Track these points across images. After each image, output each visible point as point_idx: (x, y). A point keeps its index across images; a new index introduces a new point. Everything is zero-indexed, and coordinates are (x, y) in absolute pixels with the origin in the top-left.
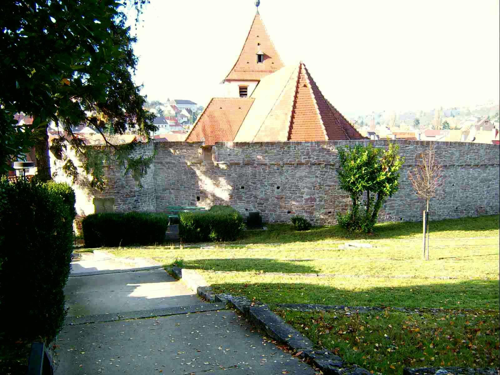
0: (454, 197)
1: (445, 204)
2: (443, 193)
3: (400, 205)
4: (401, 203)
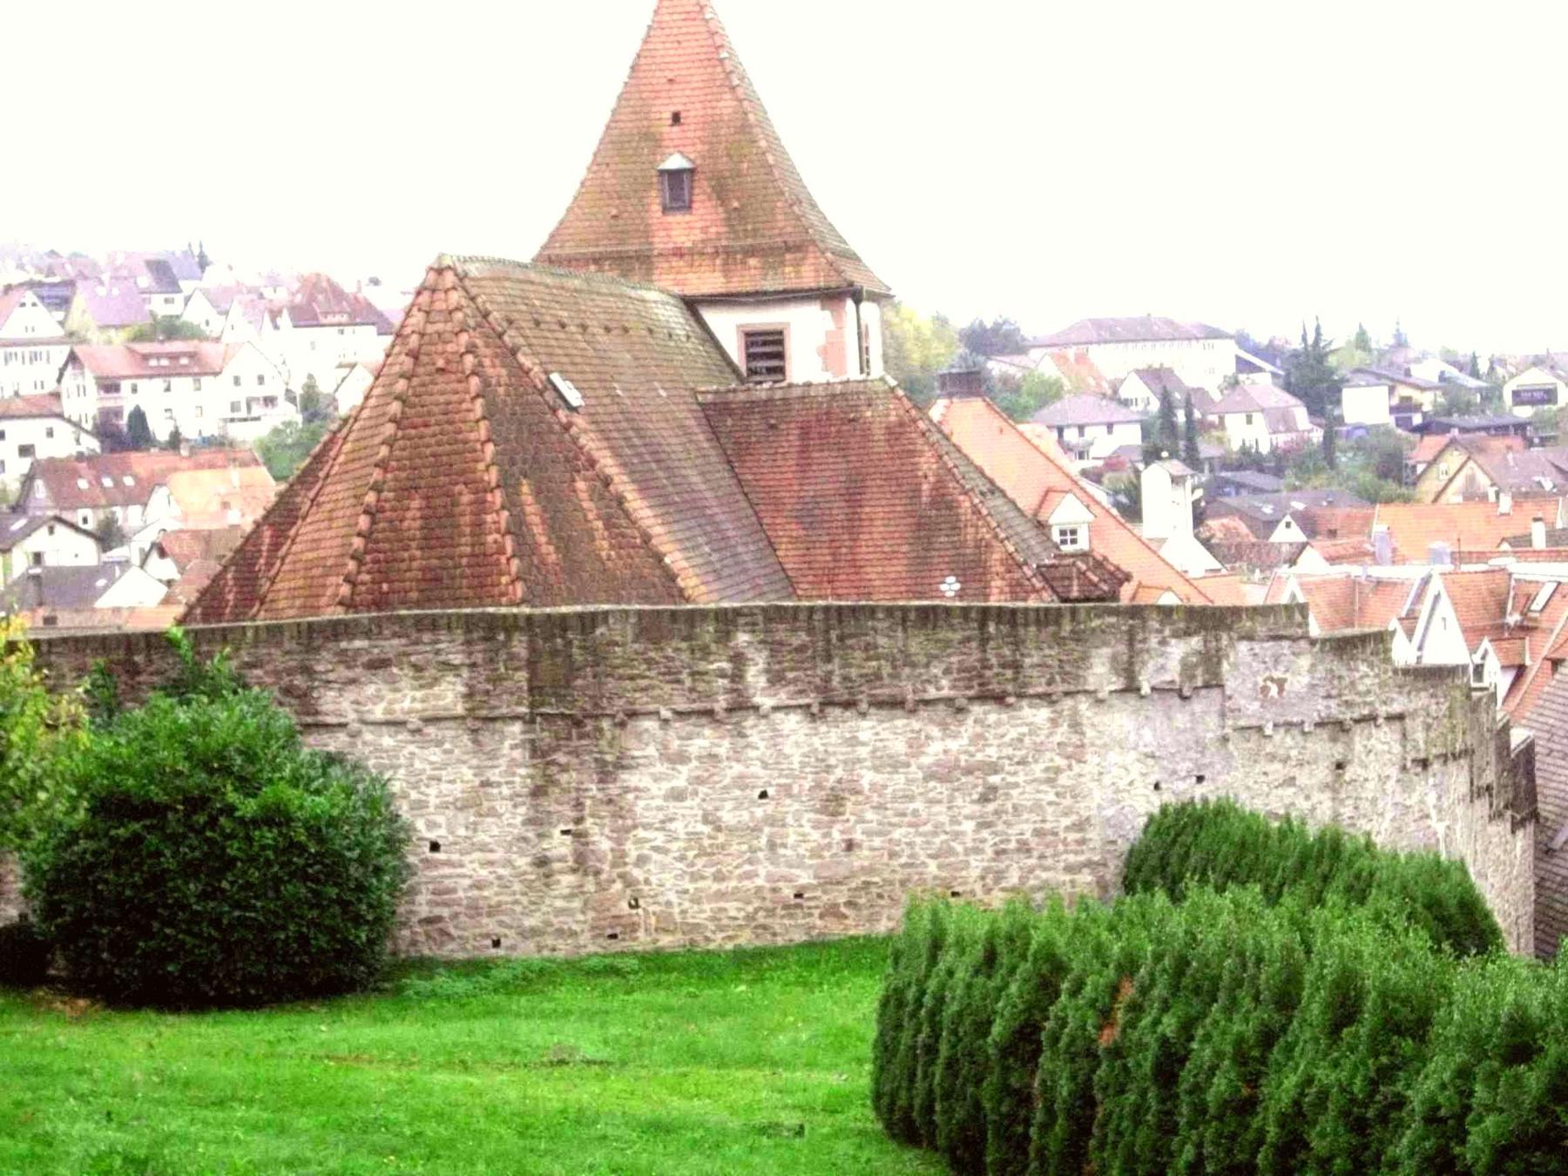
0: (772, 846)
1: (719, 877)
2: (707, 829)
3: (478, 885)
4: (484, 873)
